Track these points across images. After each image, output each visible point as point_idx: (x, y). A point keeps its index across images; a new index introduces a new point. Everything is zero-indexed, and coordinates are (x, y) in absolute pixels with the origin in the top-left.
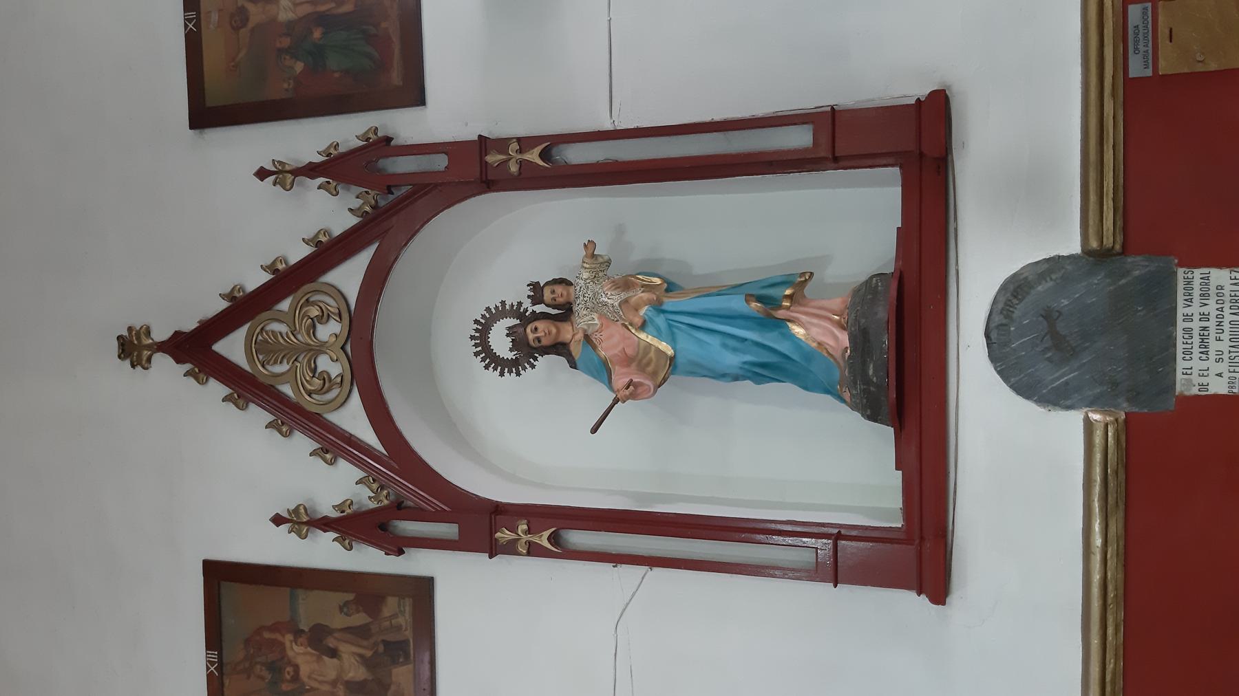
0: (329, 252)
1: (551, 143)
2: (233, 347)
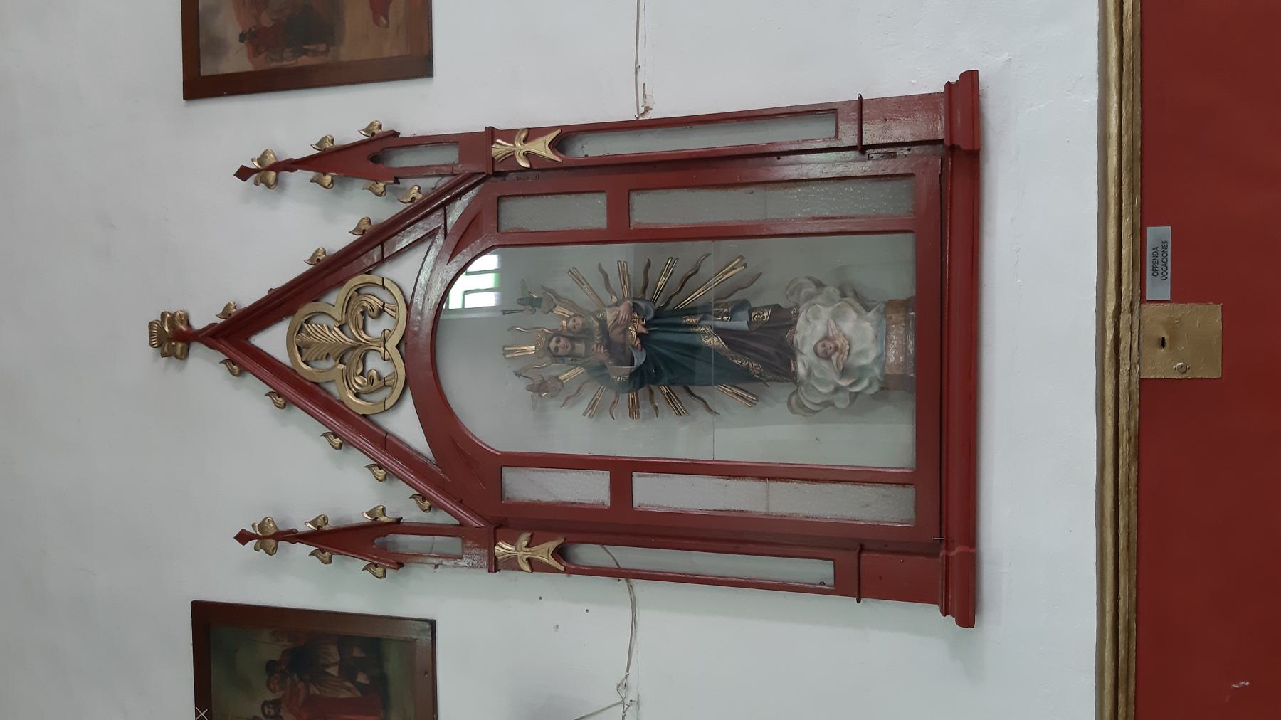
2: (273, 341)
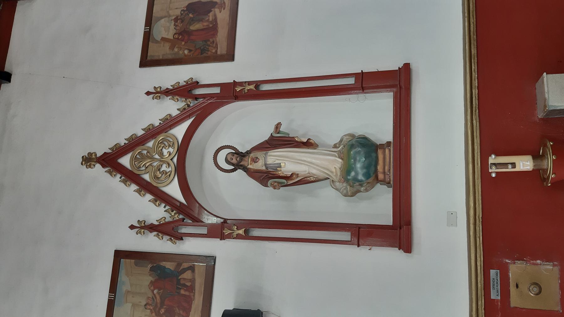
0: (170, 123)
1: (258, 84)
2: (125, 161)
